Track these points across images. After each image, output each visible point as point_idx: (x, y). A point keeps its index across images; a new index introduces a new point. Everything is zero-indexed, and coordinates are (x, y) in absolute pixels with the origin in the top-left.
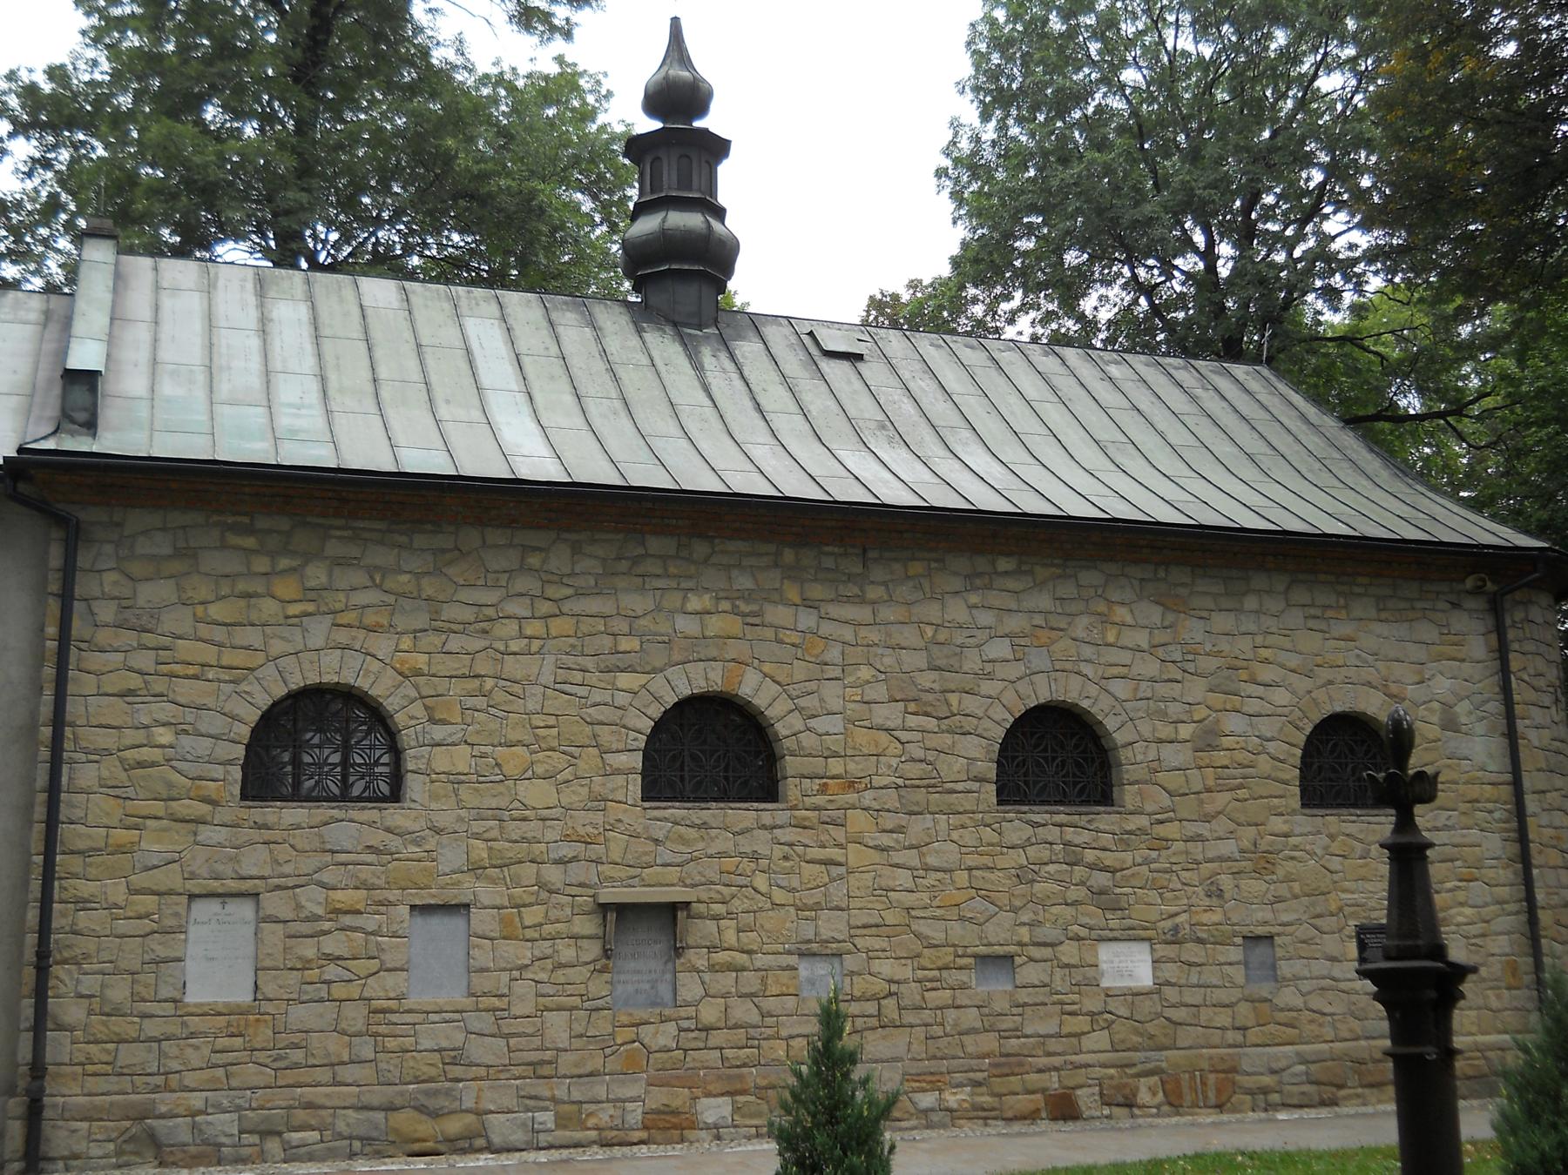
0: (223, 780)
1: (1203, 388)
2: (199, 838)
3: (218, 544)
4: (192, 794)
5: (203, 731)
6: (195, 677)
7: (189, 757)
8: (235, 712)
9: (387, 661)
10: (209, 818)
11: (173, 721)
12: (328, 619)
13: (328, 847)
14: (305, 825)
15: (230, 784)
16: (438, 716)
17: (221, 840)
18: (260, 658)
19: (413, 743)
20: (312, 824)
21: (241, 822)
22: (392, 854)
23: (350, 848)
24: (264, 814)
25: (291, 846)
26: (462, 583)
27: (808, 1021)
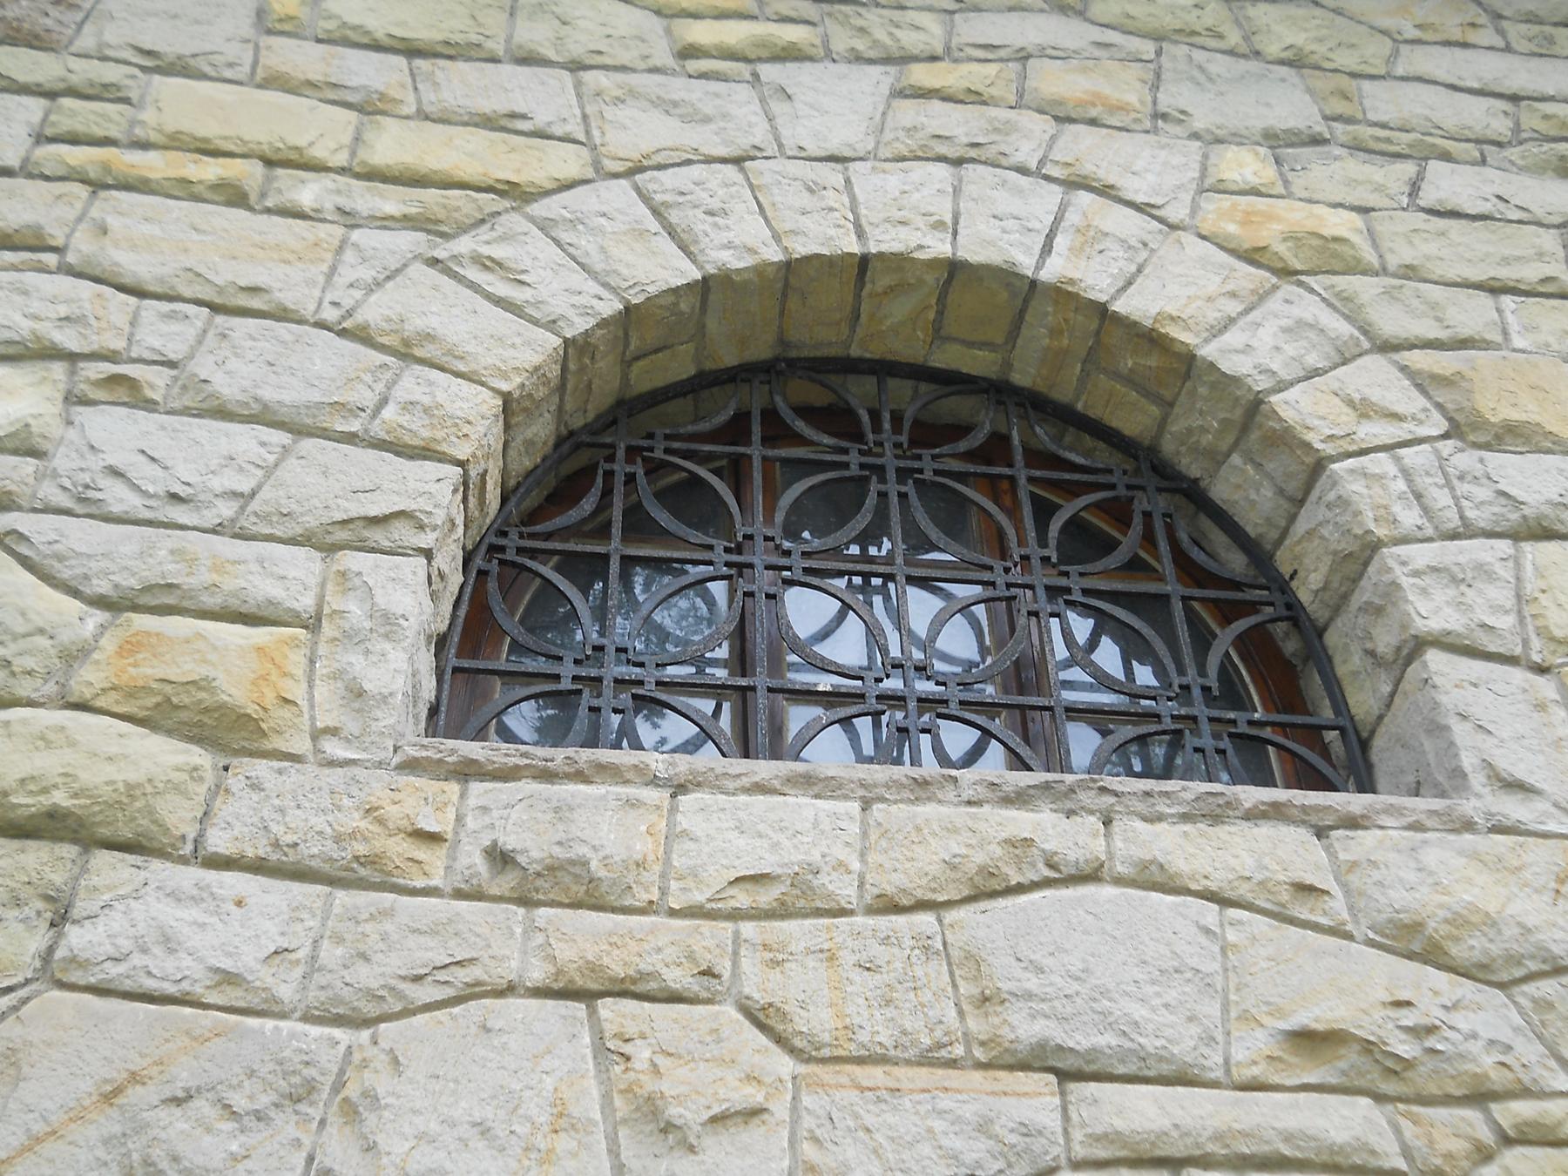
0: (313, 624)
1: (1547, 280)
2: (76, 938)
3: (319, 725)
4: (89, 679)
5: (227, 387)
6: (234, 196)
7: (118, 497)
8: (416, 323)
9: (1176, 213)
10: (179, 817)
11: (68, 339)
12: (878, 79)
13: (1025, 1028)
14: (846, 892)
15: (350, 637)
16: (1497, 408)
17: (247, 961)
18: (566, 162)
19: (1410, 518)
20: (890, 883)
21: (399, 848)
22: (1480, 1096)
23: (1184, 1045)
24: (560, 811)
25: (760, 1018)
26: (1412, 33)
27: (264, 517)
